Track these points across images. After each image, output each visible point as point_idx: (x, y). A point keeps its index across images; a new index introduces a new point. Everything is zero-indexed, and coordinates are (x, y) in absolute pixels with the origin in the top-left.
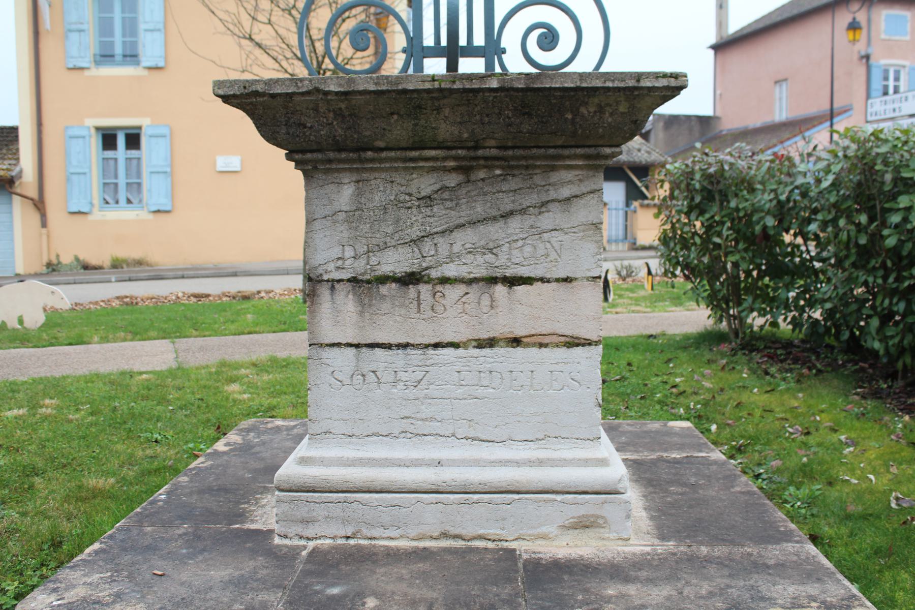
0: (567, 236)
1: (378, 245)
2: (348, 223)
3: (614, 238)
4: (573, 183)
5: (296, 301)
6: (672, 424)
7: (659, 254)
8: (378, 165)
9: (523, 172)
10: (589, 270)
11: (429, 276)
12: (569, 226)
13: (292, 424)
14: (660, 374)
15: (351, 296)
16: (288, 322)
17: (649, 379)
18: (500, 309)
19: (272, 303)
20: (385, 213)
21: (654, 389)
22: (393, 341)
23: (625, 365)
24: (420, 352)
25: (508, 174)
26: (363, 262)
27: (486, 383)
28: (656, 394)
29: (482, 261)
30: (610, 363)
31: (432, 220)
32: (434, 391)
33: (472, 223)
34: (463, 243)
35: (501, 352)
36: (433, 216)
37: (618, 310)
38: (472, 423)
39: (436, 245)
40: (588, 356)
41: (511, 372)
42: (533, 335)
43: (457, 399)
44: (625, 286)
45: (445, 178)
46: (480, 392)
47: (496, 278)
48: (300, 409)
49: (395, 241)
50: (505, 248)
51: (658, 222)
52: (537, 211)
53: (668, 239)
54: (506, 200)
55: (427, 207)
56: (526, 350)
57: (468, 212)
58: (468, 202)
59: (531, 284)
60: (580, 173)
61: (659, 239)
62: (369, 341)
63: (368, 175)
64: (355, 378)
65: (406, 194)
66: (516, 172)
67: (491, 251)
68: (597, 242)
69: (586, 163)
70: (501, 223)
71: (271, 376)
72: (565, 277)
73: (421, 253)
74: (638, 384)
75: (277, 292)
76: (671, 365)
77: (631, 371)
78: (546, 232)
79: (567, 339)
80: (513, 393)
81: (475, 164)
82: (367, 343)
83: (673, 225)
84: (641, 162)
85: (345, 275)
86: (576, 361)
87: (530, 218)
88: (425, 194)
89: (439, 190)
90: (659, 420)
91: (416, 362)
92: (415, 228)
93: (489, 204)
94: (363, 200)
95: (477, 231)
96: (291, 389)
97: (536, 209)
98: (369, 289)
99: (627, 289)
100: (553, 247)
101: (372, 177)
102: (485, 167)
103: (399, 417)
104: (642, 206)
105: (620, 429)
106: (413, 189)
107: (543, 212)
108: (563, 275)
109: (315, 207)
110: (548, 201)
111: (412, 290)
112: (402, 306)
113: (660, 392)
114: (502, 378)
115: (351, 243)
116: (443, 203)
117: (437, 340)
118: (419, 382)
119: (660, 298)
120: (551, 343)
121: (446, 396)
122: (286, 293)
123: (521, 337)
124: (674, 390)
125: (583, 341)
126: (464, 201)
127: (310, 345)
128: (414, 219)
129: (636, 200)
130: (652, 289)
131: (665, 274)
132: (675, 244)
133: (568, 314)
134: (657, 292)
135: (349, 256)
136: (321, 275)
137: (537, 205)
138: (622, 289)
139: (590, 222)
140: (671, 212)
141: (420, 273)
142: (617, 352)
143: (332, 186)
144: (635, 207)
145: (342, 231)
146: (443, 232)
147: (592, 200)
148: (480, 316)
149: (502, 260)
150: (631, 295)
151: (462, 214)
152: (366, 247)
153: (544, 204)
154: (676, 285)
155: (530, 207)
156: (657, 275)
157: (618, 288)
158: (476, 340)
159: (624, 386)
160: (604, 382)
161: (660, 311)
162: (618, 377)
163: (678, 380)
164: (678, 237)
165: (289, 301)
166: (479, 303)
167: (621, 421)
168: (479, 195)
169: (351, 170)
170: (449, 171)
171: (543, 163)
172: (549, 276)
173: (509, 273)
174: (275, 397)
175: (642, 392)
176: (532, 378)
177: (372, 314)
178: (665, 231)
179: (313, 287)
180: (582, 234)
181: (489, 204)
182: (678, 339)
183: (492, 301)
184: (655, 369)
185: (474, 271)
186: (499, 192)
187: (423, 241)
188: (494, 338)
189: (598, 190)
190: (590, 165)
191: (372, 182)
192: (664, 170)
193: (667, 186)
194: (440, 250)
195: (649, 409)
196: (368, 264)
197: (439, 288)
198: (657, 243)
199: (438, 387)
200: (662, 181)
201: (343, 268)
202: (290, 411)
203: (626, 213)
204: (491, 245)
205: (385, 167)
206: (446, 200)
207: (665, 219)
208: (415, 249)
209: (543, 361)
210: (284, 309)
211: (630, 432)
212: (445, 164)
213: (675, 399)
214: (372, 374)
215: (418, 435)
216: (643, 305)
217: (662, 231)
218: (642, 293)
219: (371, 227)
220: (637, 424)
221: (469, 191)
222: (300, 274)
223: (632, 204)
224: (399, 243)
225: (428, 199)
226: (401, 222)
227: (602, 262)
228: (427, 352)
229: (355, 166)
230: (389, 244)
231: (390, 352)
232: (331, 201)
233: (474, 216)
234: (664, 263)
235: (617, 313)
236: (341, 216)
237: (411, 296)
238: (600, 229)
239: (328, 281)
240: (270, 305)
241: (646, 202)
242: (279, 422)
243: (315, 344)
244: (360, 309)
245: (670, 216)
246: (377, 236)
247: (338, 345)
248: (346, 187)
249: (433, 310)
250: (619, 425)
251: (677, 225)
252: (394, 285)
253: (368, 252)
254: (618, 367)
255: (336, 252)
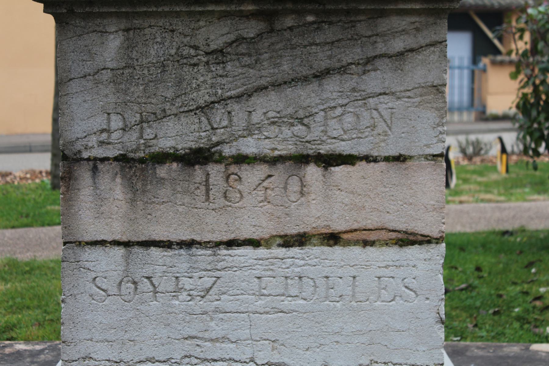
0: (399, 102)
1: (155, 114)
2: (115, 85)
3: (456, 105)
4: (407, 33)
5: (42, 187)
6: (536, 347)
7: (517, 125)
8: (155, 9)
9: (343, 18)
10: (428, 146)
11: (220, 153)
12: (402, 89)
13: (38, 347)
14: (519, 281)
15: (118, 180)
16: (31, 214)
17: (505, 289)
18: (313, 196)
19: (11, 190)
20: (164, 71)
21: (512, 302)
22: (174, 237)
23: (473, 269)
24: (209, 252)
25: (323, 22)
26: (135, 135)
27: (294, 291)
28: (514, 307)
29: (290, 134)
30: (452, 267)
31: (224, 81)
32: (226, 302)
33: (277, 85)
34: (265, 111)
35: (314, 252)
36: (226, 76)
37: (464, 198)
38: (276, 345)
39: (229, 113)
40: (427, 256)
41: (327, 277)
42: (356, 230)
43: (257, 312)
44: (472, 167)
45: (242, 26)
46: (287, 303)
47: (308, 156)
48: (48, 328)
49: (177, 108)
50: (320, 117)
51: (515, 85)
52: (360, 69)
53: (529, 106)
54: (320, 55)
55: (218, 63)
56: (347, 250)
57: (272, 71)
58: (271, 58)
59: (353, 164)
60: (417, 19)
61: (518, 107)
62: (143, 238)
63: (141, 21)
64: (123, 287)
65: (191, 47)
66: (334, 19)
67: (301, 121)
68: (437, 109)
69: (425, 6)
70: (314, 85)
71: (9, 286)
72: (397, 154)
73: (210, 123)
74: (491, 295)
75: (17, 174)
76: (533, 270)
77: (480, 277)
78: (373, 97)
79: (400, 236)
80: (329, 305)
81: (280, 8)
82: (140, 240)
83: (536, 87)
84: (492, 5)
85: (112, 152)
86: (411, 263)
87: (352, 79)
88: (216, 47)
89: (233, 42)
90: (518, 342)
91: (203, 266)
92: (203, 91)
93: (298, 61)
94: (134, 55)
95: (283, 95)
96: (35, 302)
97: (360, 67)
98: (143, 170)
99: (474, 172)
100: (382, 116)
101: (146, 25)
102: (293, 12)
103: (180, 336)
104: (494, 63)
105: (468, 354)
106: (200, 41)
107: (369, 71)
108: (394, 152)
109: (70, 63)
110: (375, 57)
111: (198, 172)
112: (186, 192)
113: (519, 305)
114: (315, 286)
115: (119, 110)
116: (238, 59)
117: (232, 237)
118: (208, 290)
119: (517, 184)
120: (378, 240)
121: (242, 309)
122: (28, 176)
123: (340, 233)
124: (538, 303)
125: (420, 238)
126: (266, 56)
127: (65, 244)
128: (202, 79)
129: (486, 55)
130: (507, 171)
131: (525, 151)
132: (539, 113)
133: (401, 203)
134: (513, 175)
135: (116, 127)
136: (80, 152)
137: (361, 62)
138: (467, 172)
139: (430, 84)
140: (533, 70)
141: (209, 150)
142: (463, 254)
143: (94, 36)
144: (485, 66)
145: (107, 95)
146: (239, 97)
147: (432, 54)
148: (287, 205)
149: (316, 133)
150: (479, 179)
151: (264, 73)
152: (138, 115)
153: (369, 60)
154: (539, 167)
155: (352, 64)
156: (513, 153)
157: (462, 169)
158: (281, 237)
159: (472, 297)
160: (447, 291)
161: (517, 200)
162: (463, 286)
163: (542, 290)
164: (542, 103)
165: (33, 186)
166: (285, 188)
167: (468, 343)
168: (285, 48)
169: (118, 15)
170: (247, 17)
171: (369, 7)
172: (376, 154)
173: (324, 149)
174: (14, 313)
175: (495, 306)
176: (354, 286)
177: (147, 202)
178: (525, 95)
179: (69, 167)
180: (418, 99)
181: (298, 61)
182: (542, 236)
183: (303, 186)
184: (512, 276)
185: (280, 147)
186: (311, 44)
187: (212, 108)
188: (305, 233)
189: (441, 43)
190: (429, 9)
191: (147, 31)
192: (524, 16)
193: (527, 37)
194: (235, 119)
195: (505, 328)
196: (141, 137)
197: (233, 168)
198: (514, 110)
199: (232, 298)
200: (522, 31)
201: (109, 143)
202: (34, 330)
203: (473, 73)
204: (301, 114)
205: (163, 11)
206: (243, 54)
207: (526, 79)
208: (203, 118)
209: (367, 264)
210: (27, 198)
211: (482, 357)
212: (242, 8)
213: (540, 315)
214: (146, 280)
215: (206, 360)
216: (496, 191)
217: (520, 95)
218: (494, 177)
219: (144, 89)
220: (490, 347)
221: (273, 44)
222: (45, 151)
223: (480, 60)
224: (182, 110)
225: (219, 54)
226: (185, 84)
227: (444, 136)
228: (219, 252)
229: (124, 10)
230: (168, 112)
231: (170, 253)
232: (92, 55)
233: (280, 76)
234: (524, 137)
235: (461, 202)
236: (106, 75)
237: (198, 180)
238: (443, 92)
239: (88, 159)
240: (8, 192)
241: (499, 58)
242: (21, 346)
243: (71, 243)
244: (129, 196)
245: (531, 75)
246: (153, 101)
247: (102, 243)
248: (112, 37)
249: (226, 197)
250: (467, 348)
251: (541, 88)
252: (175, 165)
253: (142, 122)
254: (464, 272)
255: (99, 122)
